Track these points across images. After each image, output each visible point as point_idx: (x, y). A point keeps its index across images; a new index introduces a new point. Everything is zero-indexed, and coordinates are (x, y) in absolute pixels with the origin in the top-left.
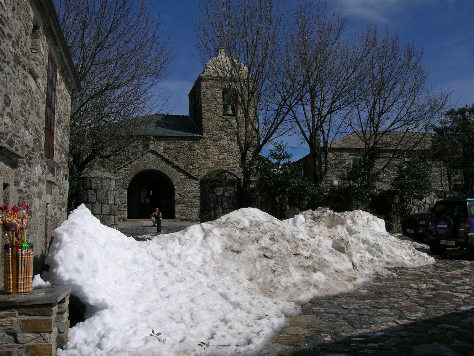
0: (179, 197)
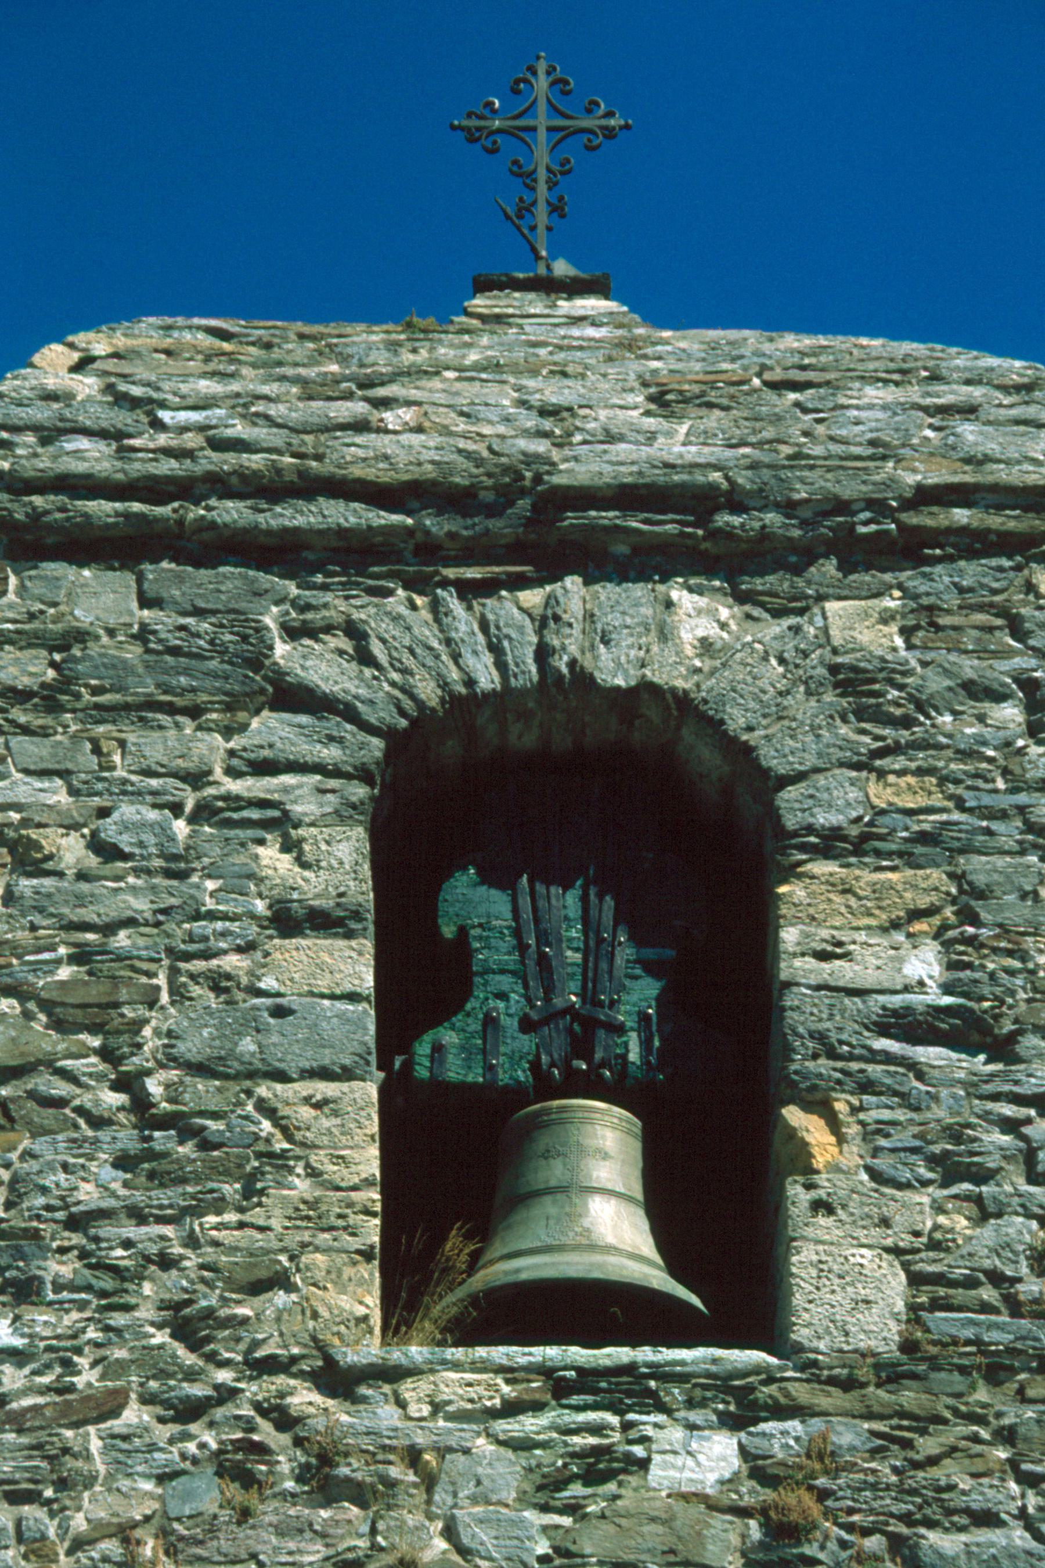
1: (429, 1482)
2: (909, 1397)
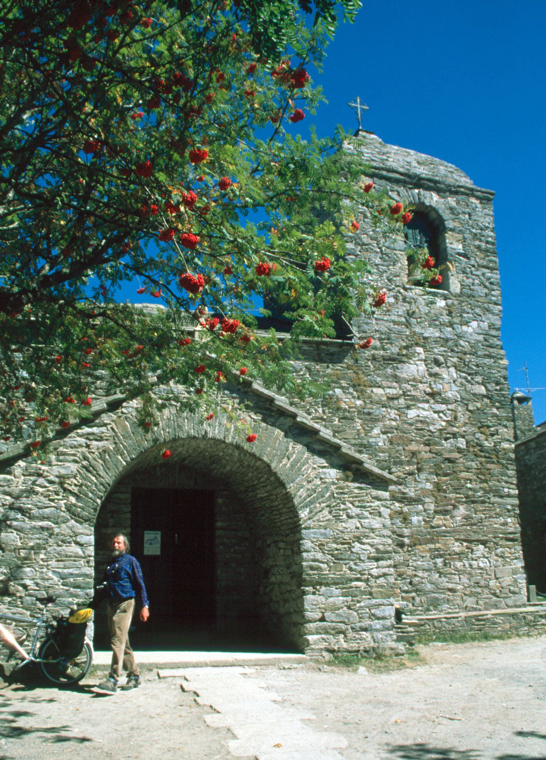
0: (319, 556)
1: (415, 302)
2: (461, 299)
